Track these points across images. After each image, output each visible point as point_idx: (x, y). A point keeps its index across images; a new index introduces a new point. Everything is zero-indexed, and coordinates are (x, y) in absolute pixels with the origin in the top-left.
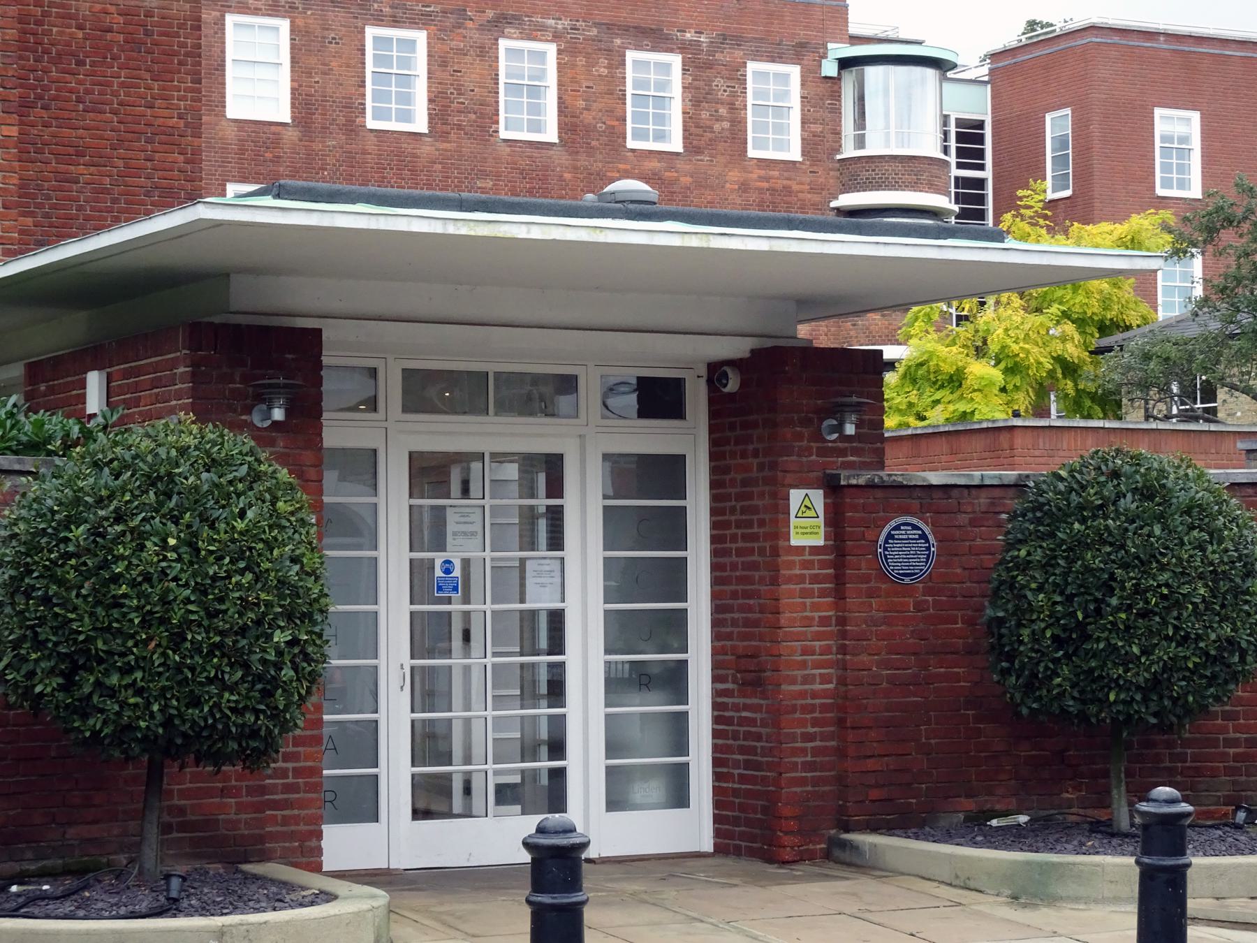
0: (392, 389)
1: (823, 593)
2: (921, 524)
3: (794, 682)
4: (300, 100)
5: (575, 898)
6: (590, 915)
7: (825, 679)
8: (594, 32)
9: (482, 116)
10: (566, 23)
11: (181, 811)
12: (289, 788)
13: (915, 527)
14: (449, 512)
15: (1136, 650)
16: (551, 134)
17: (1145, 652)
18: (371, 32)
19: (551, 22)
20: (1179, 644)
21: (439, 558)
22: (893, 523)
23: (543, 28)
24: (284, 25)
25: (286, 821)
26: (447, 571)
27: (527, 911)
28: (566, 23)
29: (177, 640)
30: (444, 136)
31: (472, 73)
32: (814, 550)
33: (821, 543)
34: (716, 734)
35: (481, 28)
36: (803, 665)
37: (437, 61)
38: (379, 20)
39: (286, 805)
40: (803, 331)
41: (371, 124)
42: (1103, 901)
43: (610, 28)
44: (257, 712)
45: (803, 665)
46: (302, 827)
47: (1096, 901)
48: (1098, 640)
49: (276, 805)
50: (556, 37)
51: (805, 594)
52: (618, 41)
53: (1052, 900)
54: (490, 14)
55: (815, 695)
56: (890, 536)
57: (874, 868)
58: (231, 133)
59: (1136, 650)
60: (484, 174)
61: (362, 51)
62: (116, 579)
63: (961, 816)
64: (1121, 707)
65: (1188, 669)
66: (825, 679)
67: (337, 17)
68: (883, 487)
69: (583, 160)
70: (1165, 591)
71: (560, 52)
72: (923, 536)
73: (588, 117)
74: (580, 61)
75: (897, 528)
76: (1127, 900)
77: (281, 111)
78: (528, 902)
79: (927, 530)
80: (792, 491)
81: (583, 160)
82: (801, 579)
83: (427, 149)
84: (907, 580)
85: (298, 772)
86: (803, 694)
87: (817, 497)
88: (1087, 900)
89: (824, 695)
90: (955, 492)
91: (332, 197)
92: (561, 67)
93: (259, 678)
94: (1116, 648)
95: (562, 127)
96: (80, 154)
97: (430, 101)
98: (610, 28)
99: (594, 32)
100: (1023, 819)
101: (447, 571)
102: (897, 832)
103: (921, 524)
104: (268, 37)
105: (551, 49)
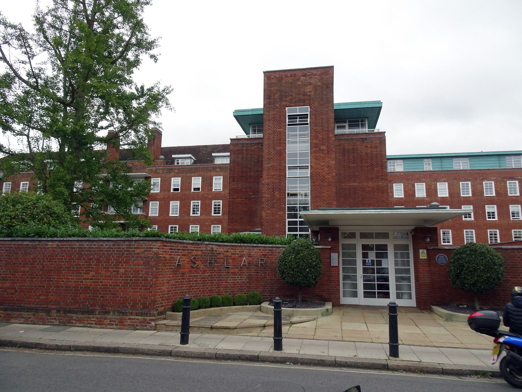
0: (358, 235)
1: (427, 266)
2: (444, 255)
3: (422, 280)
4: (450, 193)
5: (396, 314)
6: (398, 317)
7: (428, 280)
8: (501, 179)
9: (474, 194)
10: (495, 178)
11: (317, 294)
12: (335, 292)
13: (443, 256)
14: (369, 253)
15: (469, 278)
16: (494, 195)
17: (471, 278)
18: (461, 183)
19: (493, 178)
20: (478, 277)
21: (367, 259)
22: (439, 255)
23: (492, 179)
24: (447, 183)
25: (335, 296)
26: (368, 261)
27: (388, 316)
28: (495, 178)
29: (293, 270)
30: (475, 197)
31: (479, 187)
32: (425, 259)
33: (426, 258)
34: (416, 288)
35: (480, 180)
36: (424, 278)
37: (472, 186)
38: (462, 181)
39: (334, 294)
40: (425, 225)
41: (462, 196)
42: (460, 322)
43: (504, 178)
44: (305, 281)
45: (424, 278)
46: (337, 297)
47: (460, 322)
48: (463, 276)
49: (333, 294)
50: (494, 180)
51: (423, 266)
52: (505, 180)
53: (452, 321)
54: (481, 178)
55: (426, 283)
56: (438, 257)
57: (433, 312)
58: (439, 199)
59: (469, 278)
60: (482, 202)
61: (460, 186)
62: (286, 262)
63: (456, 305)
64: (469, 288)
65: (481, 281)
66: (428, 280)
67: (455, 181)
68: (436, 249)
69: (500, 198)
70: (474, 268)
71: (494, 182)
72: (445, 257)
73: (501, 192)
74: (499, 183)
75: (440, 256)
76: (465, 322)
77: (424, 195)
78: (389, 314)
79: (446, 256)
80: (420, 250)
81: (500, 198)
82: (423, 264)
83: (472, 199)
84: (442, 264)
85: (336, 289)
86: (423, 282)
87: (425, 251)
88: (458, 321)
89: (428, 282)
90: (451, 250)
91: (326, 210)
92: (495, 185)
93: (305, 276)
94: (466, 278)
95: (496, 193)
96: (371, 205)
97: (472, 192)
98: (504, 178)
99: (501, 179)
100: (465, 306)
101: (368, 261)
102: (442, 306)
103: (444, 255)
104: (400, 187)
105: (493, 182)
